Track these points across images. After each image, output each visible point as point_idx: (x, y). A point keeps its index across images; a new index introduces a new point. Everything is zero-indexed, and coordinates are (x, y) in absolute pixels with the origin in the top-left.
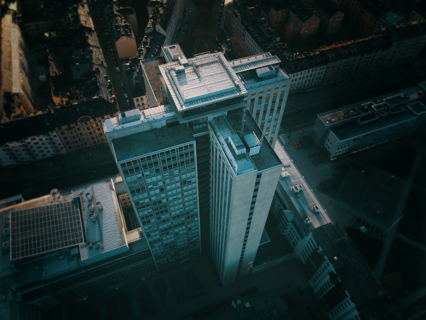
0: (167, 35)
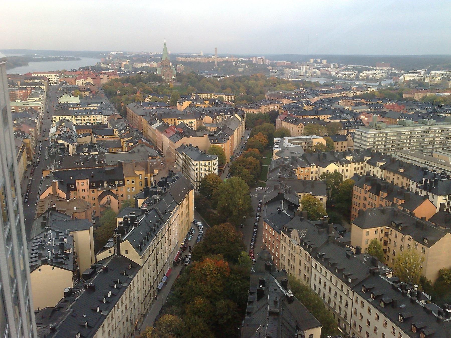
0: (144, 264)
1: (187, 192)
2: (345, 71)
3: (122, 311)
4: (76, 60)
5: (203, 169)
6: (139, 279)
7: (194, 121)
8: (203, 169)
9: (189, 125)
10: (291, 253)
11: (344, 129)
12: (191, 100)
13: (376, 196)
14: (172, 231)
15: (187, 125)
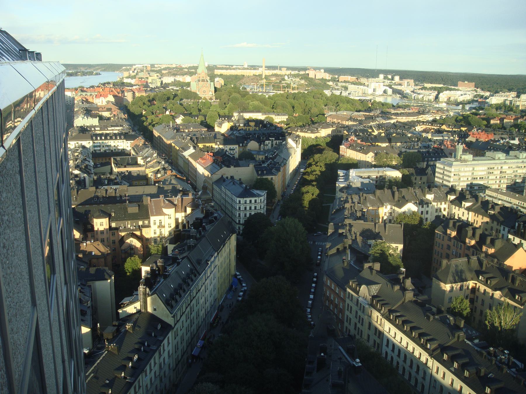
0: (175, 324)
1: (227, 237)
2: (422, 90)
3: (151, 379)
4: (95, 75)
5: (248, 208)
6: (170, 341)
7: (236, 147)
8: (248, 208)
9: (229, 152)
10: (358, 314)
11: (423, 161)
12: (233, 121)
13: (462, 244)
14: (195, 306)
15: (227, 152)
